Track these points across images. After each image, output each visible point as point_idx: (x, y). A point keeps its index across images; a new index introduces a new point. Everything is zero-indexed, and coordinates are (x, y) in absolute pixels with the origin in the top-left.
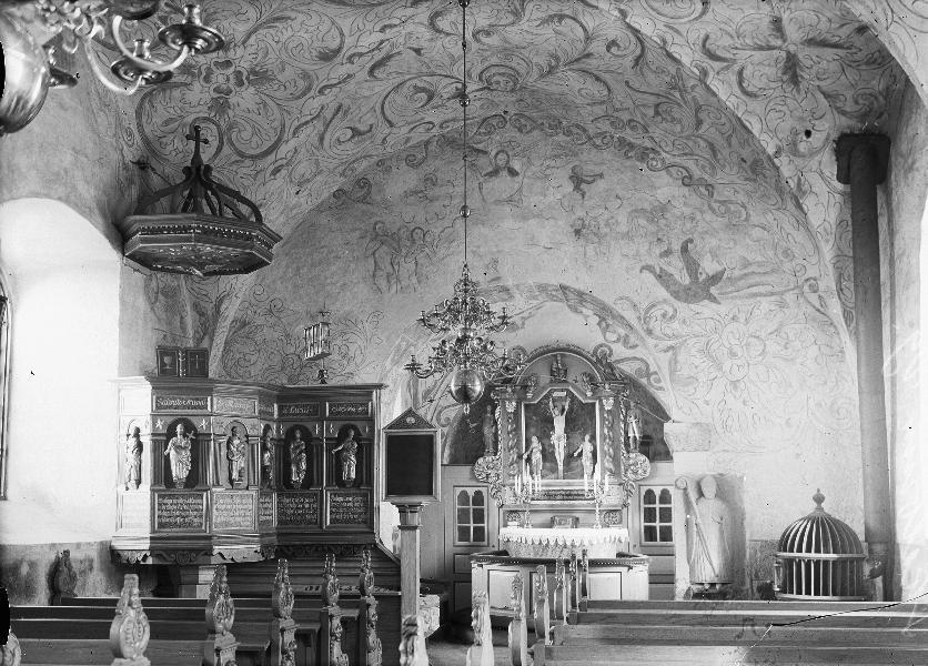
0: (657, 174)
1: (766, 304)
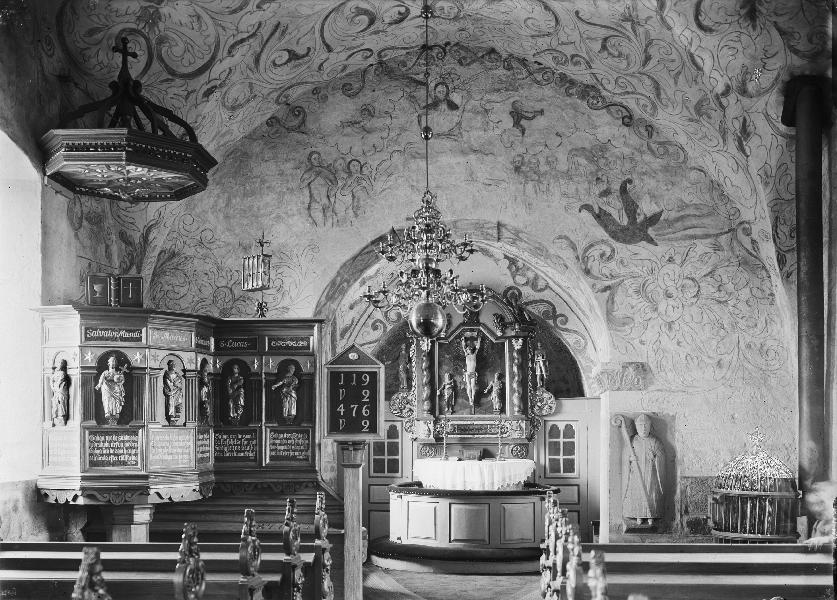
0: (598, 112)
1: (702, 247)
